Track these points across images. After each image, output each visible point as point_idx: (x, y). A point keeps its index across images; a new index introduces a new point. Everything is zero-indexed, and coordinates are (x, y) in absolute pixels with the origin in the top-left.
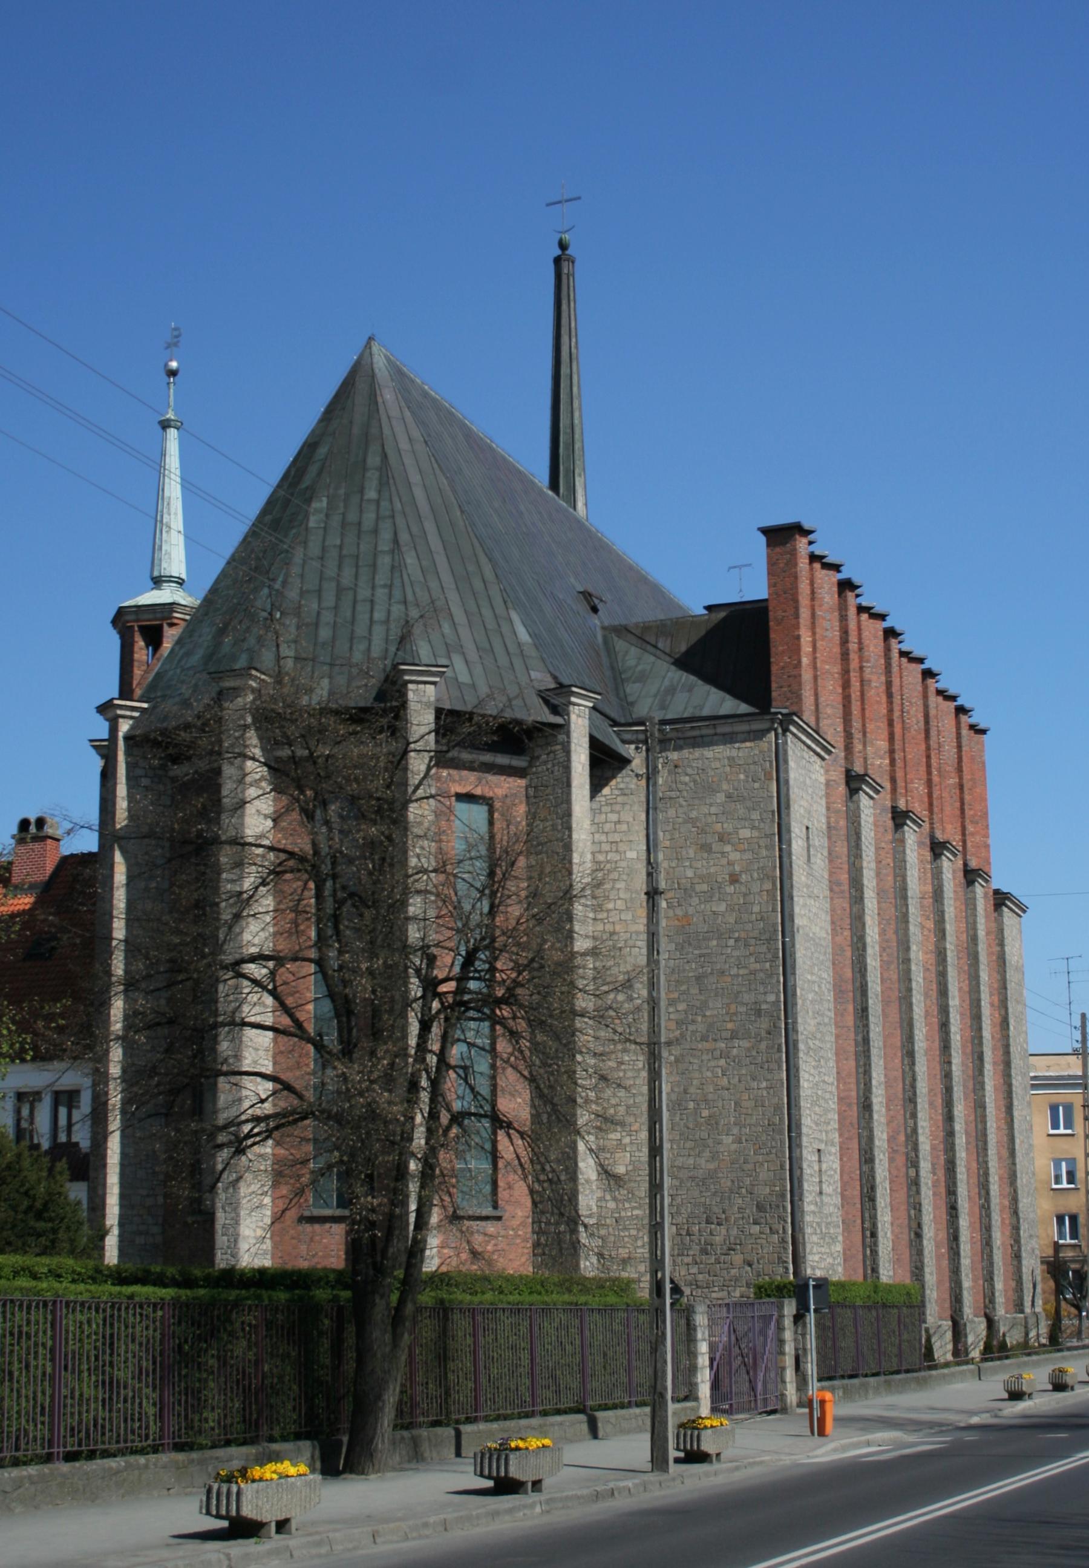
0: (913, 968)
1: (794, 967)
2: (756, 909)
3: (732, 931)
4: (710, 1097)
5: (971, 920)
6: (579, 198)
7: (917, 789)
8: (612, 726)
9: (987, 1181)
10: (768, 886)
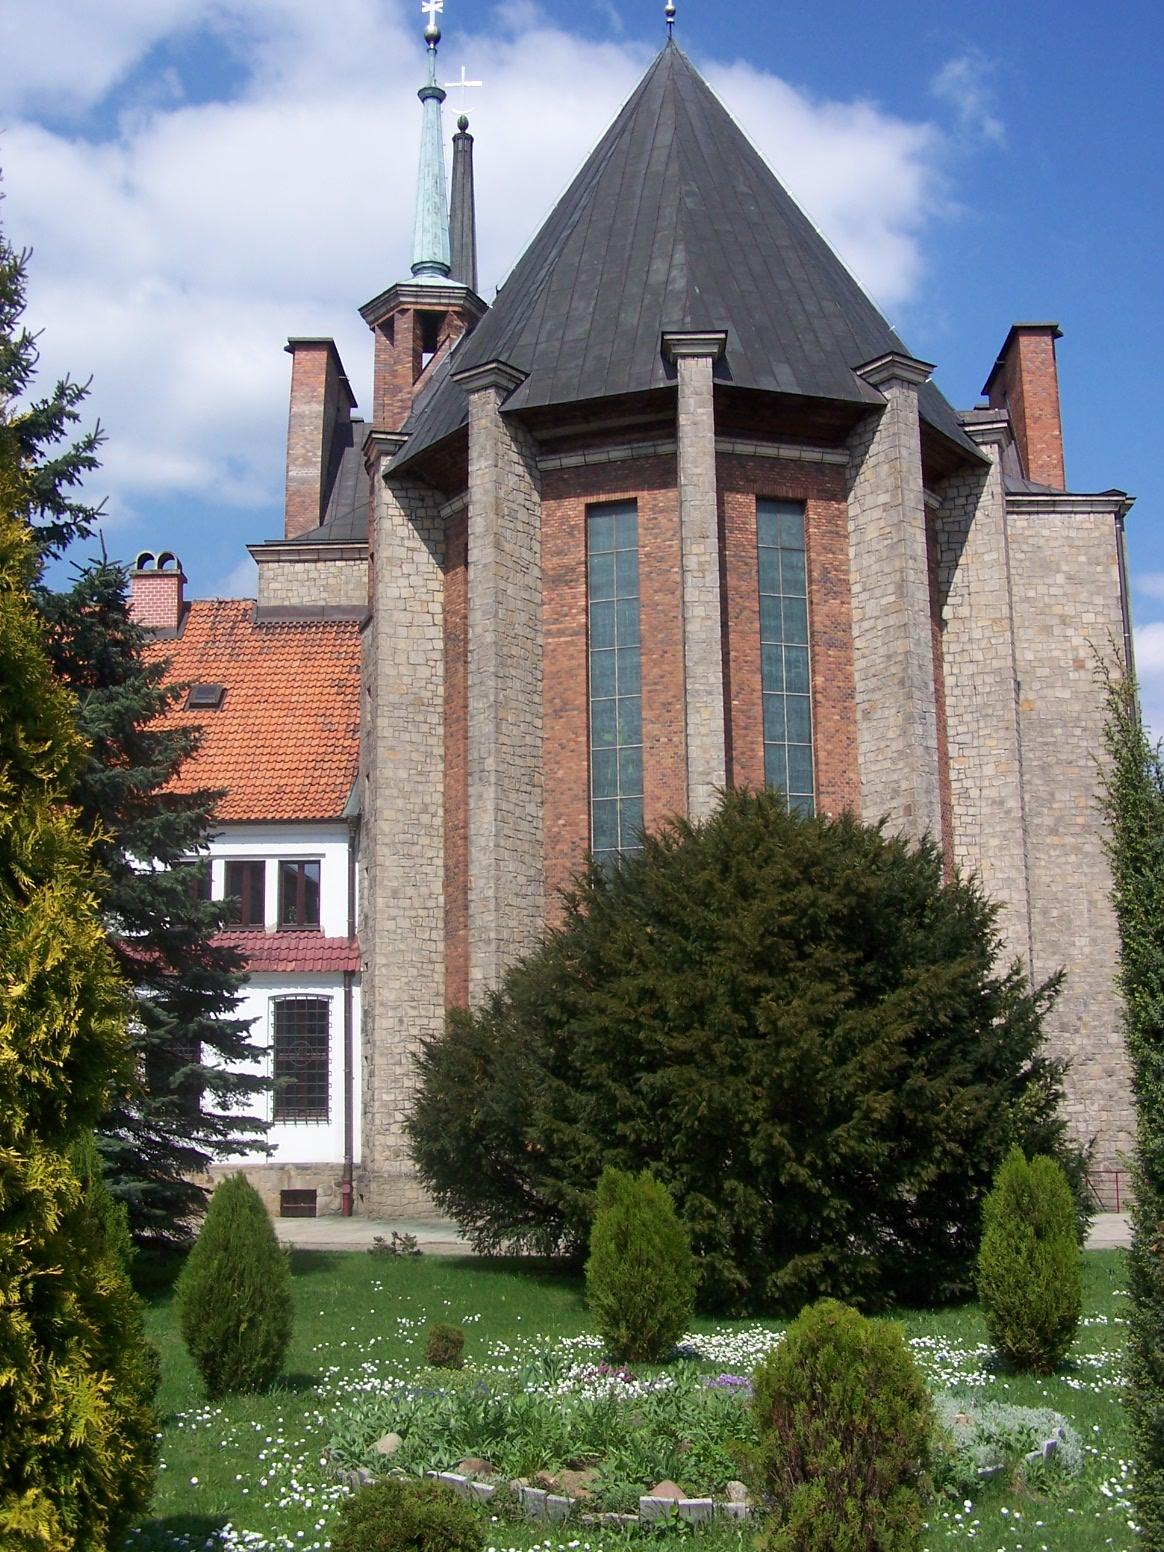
3: (1078, 719)
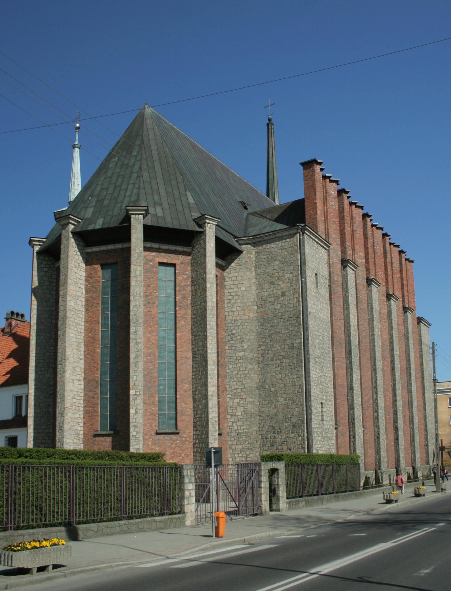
0: (376, 337)
1: (307, 328)
2: (292, 306)
4: (274, 383)
5: (406, 325)
6: (274, 104)
7: (381, 275)
8: (234, 238)
9: (413, 418)
10: (296, 296)
